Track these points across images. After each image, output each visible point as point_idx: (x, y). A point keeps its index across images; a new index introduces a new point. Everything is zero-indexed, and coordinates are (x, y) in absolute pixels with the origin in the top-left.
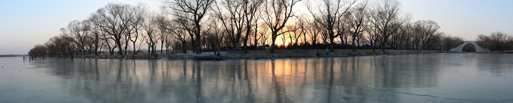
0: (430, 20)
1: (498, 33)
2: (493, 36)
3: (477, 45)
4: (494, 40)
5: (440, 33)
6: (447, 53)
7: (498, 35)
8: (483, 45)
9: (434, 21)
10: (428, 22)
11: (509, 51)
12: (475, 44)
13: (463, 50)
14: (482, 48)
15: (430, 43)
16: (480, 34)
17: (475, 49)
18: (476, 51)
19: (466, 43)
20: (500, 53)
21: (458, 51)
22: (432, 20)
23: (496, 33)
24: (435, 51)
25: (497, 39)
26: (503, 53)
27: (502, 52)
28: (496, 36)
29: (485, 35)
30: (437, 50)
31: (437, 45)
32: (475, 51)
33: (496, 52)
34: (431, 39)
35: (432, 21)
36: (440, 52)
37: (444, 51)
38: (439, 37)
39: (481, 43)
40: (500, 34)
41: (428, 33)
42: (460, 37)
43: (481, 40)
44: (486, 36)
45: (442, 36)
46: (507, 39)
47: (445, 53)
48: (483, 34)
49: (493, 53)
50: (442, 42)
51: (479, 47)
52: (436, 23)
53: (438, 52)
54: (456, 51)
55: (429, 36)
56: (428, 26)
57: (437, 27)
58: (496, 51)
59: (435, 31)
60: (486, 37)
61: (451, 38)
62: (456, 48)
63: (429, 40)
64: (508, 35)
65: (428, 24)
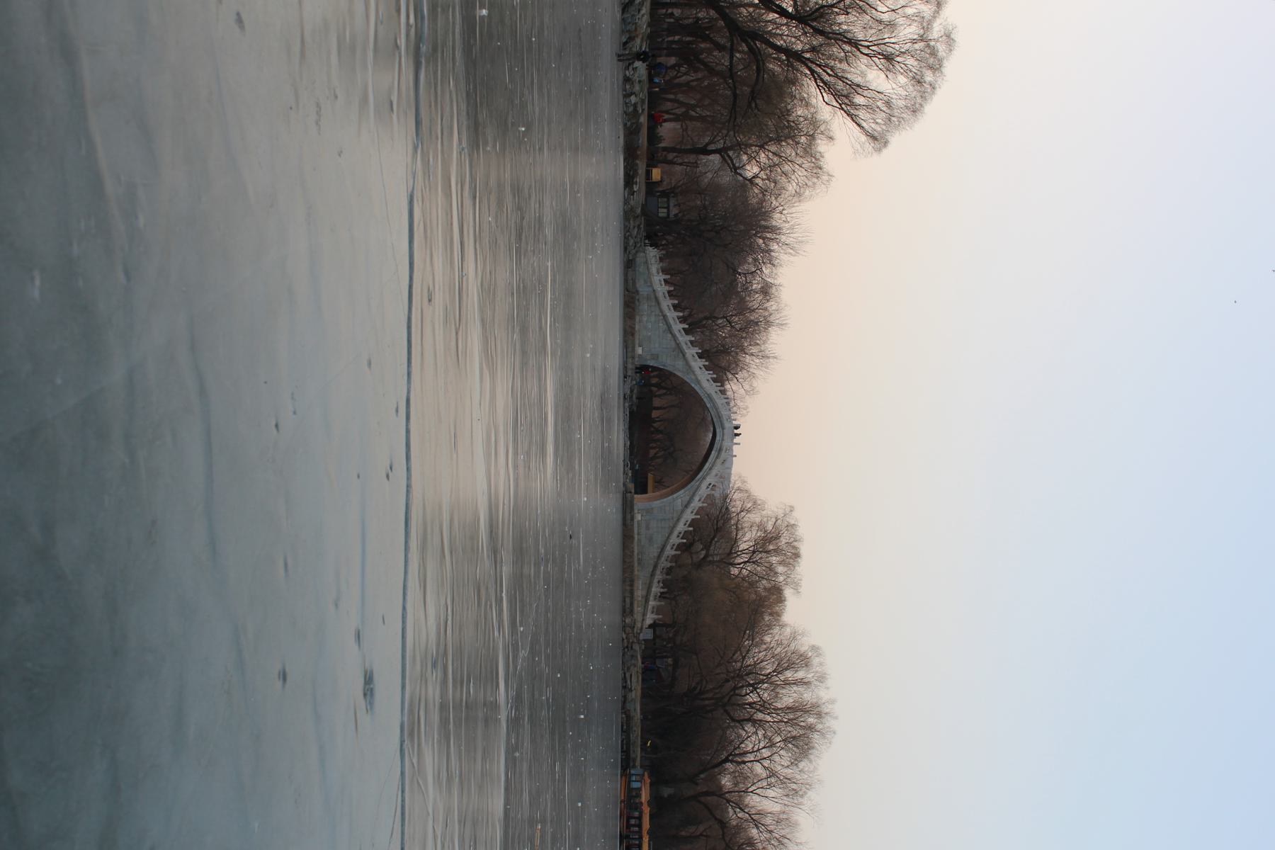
0: (957, 53)
1: (819, 715)
2: (791, 666)
3: (696, 504)
4: (753, 670)
5: (822, 146)
6: (628, 215)
7: (799, 709)
8: (699, 565)
9: (940, 93)
10: (936, 31)
11: (646, 824)
12: (704, 487)
13: (643, 369)
14: (669, 552)
15: (720, 48)
16: (801, 531)
17: (659, 484)
18: (640, 501)
19: (720, 401)
20: (626, 730)
21: (646, 322)
22: (952, 66)
23: (821, 694)
24: (640, 95)
25: (764, 706)
26: (626, 764)
27: (637, 753)
28: (788, 697)
29: (796, 587)
30: (654, 121)
31: (701, 118)
32: (642, 488)
33: (636, 694)
34: (757, 58)
35: (936, 68)
36: (630, 153)
37: (639, 186)
38: (778, 140)
39: (718, 550)
40: (811, 728)
41: (822, 33)
42: (776, 341)
43: (746, 541)
44: (788, 593)
45: (787, 168)
46: (765, 801)
47: (626, 202)
48: (805, 568)
49: (626, 667)
50: (735, 169)
51: (681, 527)
52: (915, 110)
53: (631, 132)
54: (644, 307)
55: (793, 37)
56: (891, 25)
57: (880, 117)
58: (644, 696)
59: (845, 95)
60: (776, 594)
61: (769, 251)
62: (667, 303)
63: (754, 37)
64: (800, 816)
65: (908, 31)
